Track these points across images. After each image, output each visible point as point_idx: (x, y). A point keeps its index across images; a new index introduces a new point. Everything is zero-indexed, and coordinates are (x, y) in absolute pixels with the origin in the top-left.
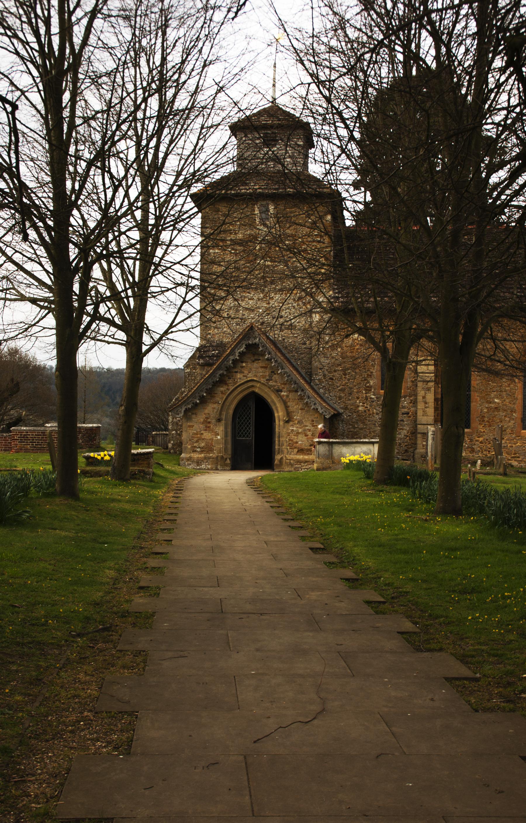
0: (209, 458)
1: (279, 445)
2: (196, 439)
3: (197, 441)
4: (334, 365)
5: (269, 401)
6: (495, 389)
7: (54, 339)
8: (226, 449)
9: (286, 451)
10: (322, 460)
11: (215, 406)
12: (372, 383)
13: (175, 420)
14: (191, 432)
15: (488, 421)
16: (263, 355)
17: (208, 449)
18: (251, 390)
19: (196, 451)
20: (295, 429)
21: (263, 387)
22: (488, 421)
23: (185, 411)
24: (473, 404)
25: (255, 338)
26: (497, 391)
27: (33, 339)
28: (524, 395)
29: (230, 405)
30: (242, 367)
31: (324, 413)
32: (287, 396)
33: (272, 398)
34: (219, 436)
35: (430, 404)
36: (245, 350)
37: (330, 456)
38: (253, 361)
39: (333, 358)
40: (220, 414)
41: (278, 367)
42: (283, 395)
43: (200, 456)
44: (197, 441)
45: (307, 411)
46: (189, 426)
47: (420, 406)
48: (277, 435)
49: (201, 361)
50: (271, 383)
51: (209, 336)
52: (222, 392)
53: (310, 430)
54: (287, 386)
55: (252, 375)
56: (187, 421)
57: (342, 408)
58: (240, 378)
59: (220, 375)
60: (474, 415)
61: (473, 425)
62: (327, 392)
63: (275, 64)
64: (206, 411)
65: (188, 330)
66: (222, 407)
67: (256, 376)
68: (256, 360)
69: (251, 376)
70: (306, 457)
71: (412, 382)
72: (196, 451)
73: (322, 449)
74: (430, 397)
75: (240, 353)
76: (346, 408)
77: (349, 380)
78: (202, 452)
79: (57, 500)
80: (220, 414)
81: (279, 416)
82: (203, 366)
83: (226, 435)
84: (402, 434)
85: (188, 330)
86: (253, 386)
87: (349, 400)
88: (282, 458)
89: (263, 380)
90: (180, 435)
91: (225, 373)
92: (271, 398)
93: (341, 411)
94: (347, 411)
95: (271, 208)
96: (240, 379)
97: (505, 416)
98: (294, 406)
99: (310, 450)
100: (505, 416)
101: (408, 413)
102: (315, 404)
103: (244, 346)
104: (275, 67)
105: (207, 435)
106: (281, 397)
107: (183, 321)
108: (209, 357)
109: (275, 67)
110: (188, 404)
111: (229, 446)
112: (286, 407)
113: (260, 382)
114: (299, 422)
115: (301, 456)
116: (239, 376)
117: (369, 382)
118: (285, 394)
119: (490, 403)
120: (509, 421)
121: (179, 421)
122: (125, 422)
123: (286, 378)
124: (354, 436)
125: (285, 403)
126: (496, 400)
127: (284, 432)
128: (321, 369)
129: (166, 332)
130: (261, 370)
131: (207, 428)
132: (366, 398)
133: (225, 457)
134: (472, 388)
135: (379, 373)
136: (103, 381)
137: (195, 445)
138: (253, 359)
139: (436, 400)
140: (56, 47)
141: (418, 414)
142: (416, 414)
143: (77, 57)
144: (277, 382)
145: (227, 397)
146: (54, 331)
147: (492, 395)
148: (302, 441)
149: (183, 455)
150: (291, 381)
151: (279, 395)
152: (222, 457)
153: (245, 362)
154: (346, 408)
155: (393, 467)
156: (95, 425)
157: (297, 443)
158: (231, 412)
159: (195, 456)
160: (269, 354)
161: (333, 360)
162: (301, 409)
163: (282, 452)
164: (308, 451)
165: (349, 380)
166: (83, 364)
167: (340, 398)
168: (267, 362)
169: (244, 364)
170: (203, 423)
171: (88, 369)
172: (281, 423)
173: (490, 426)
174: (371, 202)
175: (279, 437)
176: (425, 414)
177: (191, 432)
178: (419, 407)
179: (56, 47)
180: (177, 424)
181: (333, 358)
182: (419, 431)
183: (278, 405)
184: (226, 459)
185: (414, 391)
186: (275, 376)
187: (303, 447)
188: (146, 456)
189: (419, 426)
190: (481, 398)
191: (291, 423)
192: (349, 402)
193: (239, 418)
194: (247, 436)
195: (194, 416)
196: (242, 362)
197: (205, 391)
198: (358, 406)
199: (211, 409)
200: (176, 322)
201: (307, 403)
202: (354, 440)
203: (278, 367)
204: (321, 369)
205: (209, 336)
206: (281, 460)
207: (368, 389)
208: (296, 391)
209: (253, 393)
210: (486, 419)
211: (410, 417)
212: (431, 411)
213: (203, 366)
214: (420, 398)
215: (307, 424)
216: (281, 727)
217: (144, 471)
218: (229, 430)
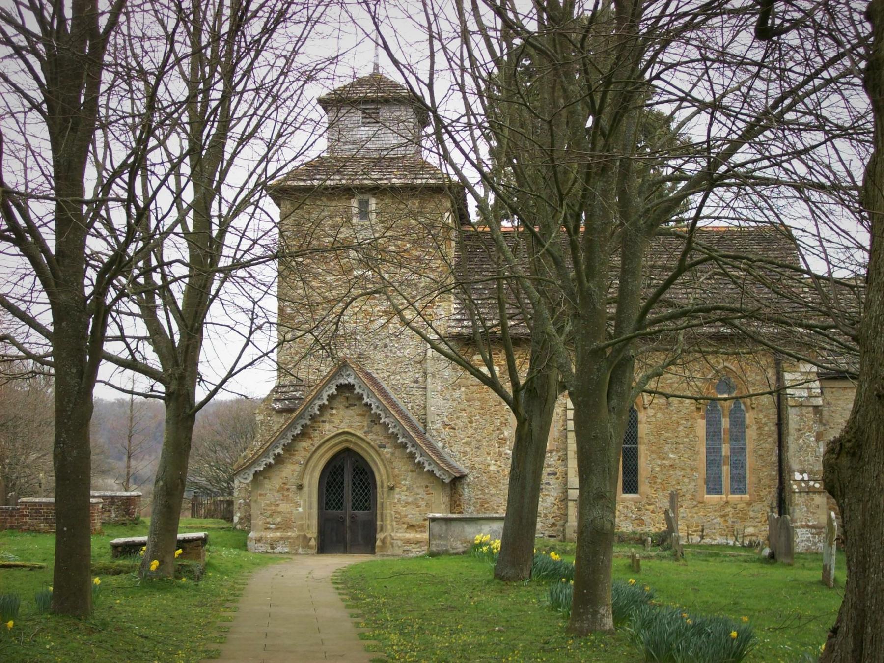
0: (288, 538)
2: (269, 512)
3: (271, 516)
12: (506, 433)
19: (269, 529)
30: (332, 415)
36: (335, 393)
44: (271, 516)
52: (305, 449)
58: (328, 429)
67: (350, 427)
70: (418, 536)
76: (473, 468)
77: (476, 429)
84: (548, 501)
86: (346, 441)
96: (329, 431)
101: (555, 474)
105: (284, 507)
116: (327, 426)
119: (664, 459)
120: (689, 483)
126: (671, 456)
131: (286, 498)
132: (500, 455)
134: (639, 440)
137: (268, 520)
141: (569, 475)
142: (566, 474)
154: (473, 468)
159: (270, 535)
165: (476, 429)
169: (334, 411)
170: (278, 491)
173: (664, 490)
184: (310, 539)
187: (414, 523)
195: (266, 481)
196: (332, 408)
199: (289, 471)
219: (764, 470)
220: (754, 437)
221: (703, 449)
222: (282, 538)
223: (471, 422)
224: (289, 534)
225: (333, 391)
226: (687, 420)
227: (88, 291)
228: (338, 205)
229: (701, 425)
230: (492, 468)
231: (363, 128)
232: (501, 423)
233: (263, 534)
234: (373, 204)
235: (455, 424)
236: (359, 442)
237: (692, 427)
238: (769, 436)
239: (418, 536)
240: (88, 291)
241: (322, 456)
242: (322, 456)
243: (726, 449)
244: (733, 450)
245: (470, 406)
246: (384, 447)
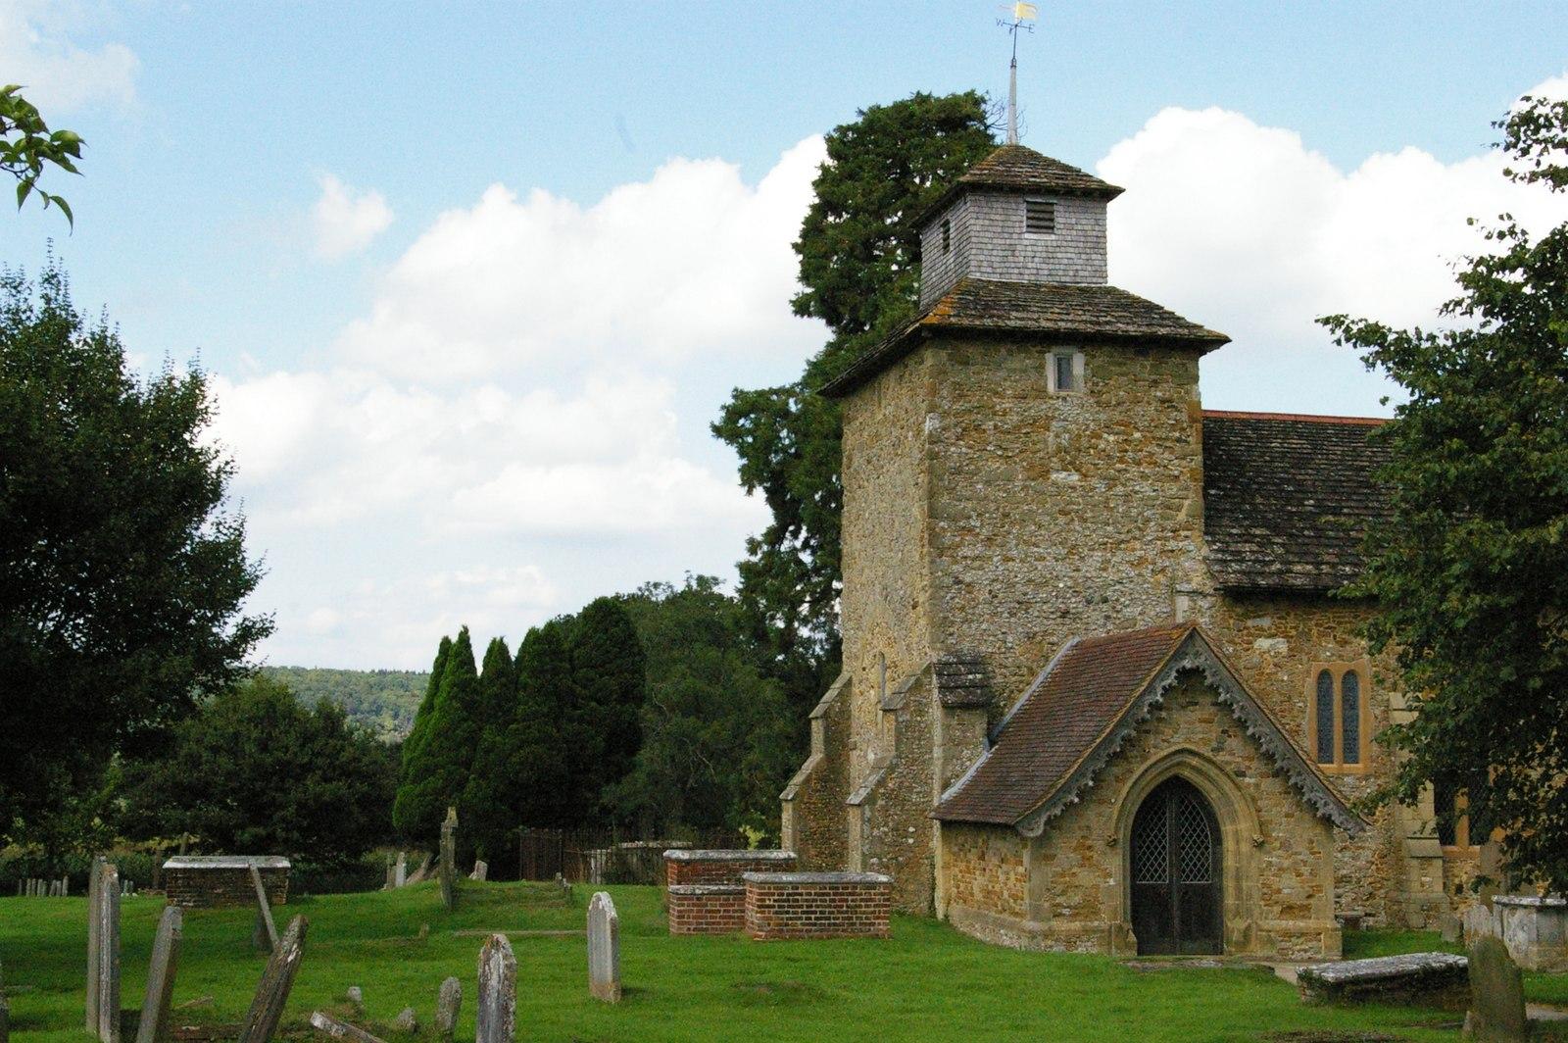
0: (1095, 931)
1: (1238, 897)
2: (1060, 888)
19: (1060, 915)
32: (1257, 786)
44: (1063, 893)
51: (951, 640)
53: (1305, 863)
55: (1189, 732)
63: (1014, 60)
70: (1301, 924)
72: (1060, 915)
78: (1074, 916)
88: (1249, 927)
99: (1307, 908)
104: (1013, 66)
105: (1086, 878)
109: (1013, 66)
115: (1291, 923)
118: (1253, 781)
130: (1199, 727)
131: (1086, 862)
148: (1290, 887)
152: (1120, 928)
157: (1279, 891)
162: (1287, 815)
163: (1249, 913)
164: (1303, 910)
170: (1075, 850)
172: (1245, 847)
175: (1238, 879)
197: (1090, 775)
205: (951, 640)
206: (1246, 934)
209: (1176, 778)
215: (1300, 849)
222: (1086, 931)
224: (1096, 923)
225: (1171, 680)
228: (1020, 361)
231: (1027, 236)
233: (1055, 924)
234: (1078, 364)
236: (1206, 767)
239: (1301, 924)
246: (1243, 774)
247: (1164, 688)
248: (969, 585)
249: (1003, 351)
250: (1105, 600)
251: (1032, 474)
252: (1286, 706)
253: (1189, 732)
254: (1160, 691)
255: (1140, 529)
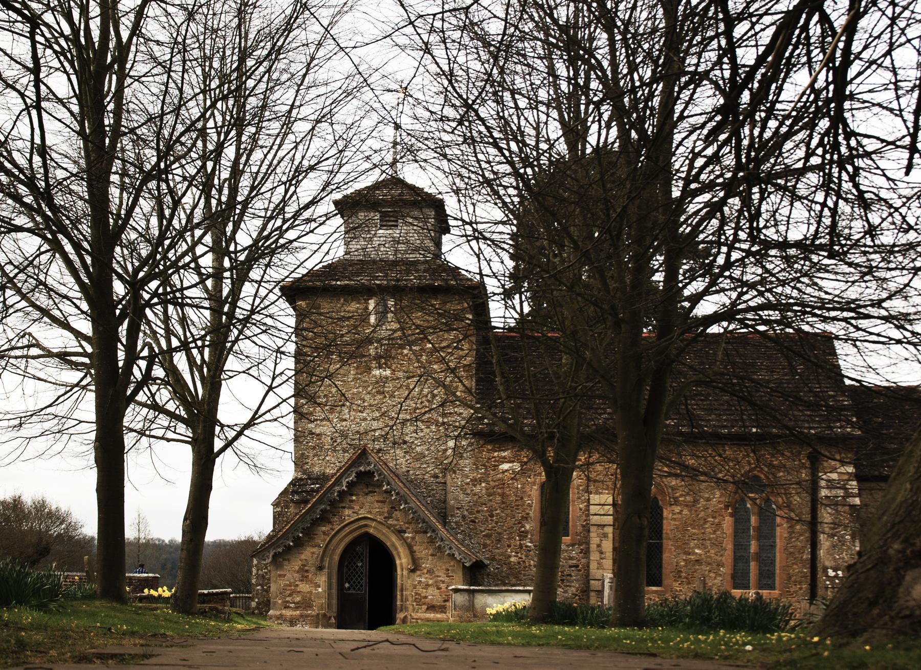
0: (307, 616)
1: (402, 601)
2: (289, 592)
4: (476, 503)
5: (388, 544)
6: (695, 537)
7: (93, 436)
8: (329, 605)
9: (411, 607)
10: (460, 612)
11: (315, 550)
12: (528, 527)
13: (260, 572)
14: (282, 582)
15: (686, 578)
16: (381, 486)
17: (306, 604)
18: (363, 530)
19: (289, 607)
20: (423, 580)
21: (380, 527)
22: (686, 578)
23: (274, 557)
24: (665, 556)
25: (369, 464)
26: (699, 540)
27: (66, 437)
28: (735, 545)
29: (334, 550)
30: (352, 501)
31: (463, 560)
32: (413, 538)
33: (392, 541)
34: (319, 588)
35: (607, 554)
36: (355, 480)
37: (471, 607)
38: (367, 494)
39: (475, 495)
40: (322, 560)
41: (400, 501)
42: (408, 537)
43: (294, 613)
44: (290, 595)
45: (440, 558)
46: (280, 576)
47: (594, 556)
48: (399, 588)
49: (296, 497)
50: (390, 522)
52: (324, 533)
54: (413, 526)
55: (364, 510)
56: (277, 569)
57: (487, 559)
58: (348, 514)
59: (322, 510)
60: (667, 569)
61: (666, 582)
62: (467, 538)
64: (303, 557)
65: (275, 420)
66: (324, 552)
67: (370, 512)
68: (370, 492)
69: (363, 513)
70: (439, 616)
71: (583, 526)
72: (289, 607)
73: (460, 599)
74: (608, 546)
75: (348, 482)
76: (493, 559)
77: (496, 523)
78: (296, 608)
79: (97, 603)
80: (322, 560)
81: (401, 564)
82: (298, 503)
83: (330, 587)
84: (570, 592)
85: (275, 420)
86: (366, 526)
87: (497, 548)
88: (406, 617)
89: (379, 518)
90: (268, 591)
91: (328, 508)
92: (390, 540)
93: (487, 562)
94: (494, 563)
95: (391, 303)
96: (349, 516)
97: (710, 571)
98: (422, 551)
100: (710, 571)
101: (577, 566)
102: (451, 548)
103: (354, 474)
105: (304, 587)
106: (405, 540)
107: (269, 411)
108: (306, 492)
110: (278, 547)
111: (334, 602)
112: (412, 552)
113: (376, 520)
114: (428, 571)
116: (347, 512)
117: (524, 526)
118: (410, 535)
119: (689, 554)
120: (715, 578)
121: (266, 573)
122: (191, 540)
123: (411, 516)
124: (505, 581)
125: (410, 547)
126: (697, 551)
127: (408, 583)
128: (458, 509)
129: (248, 426)
130: (377, 505)
131: (304, 578)
132: (521, 546)
133: (328, 615)
134: (664, 536)
135: (538, 515)
136: (164, 556)
137: (287, 599)
138: (367, 491)
139: (614, 549)
140: (96, 34)
141: (591, 567)
142: (588, 567)
143: (123, 50)
144: (399, 519)
145: (332, 539)
146: (94, 426)
147: (692, 544)
148: (433, 595)
149: (271, 612)
150: (418, 519)
151: (403, 537)
152: (325, 615)
153: (356, 495)
154: (493, 559)
155: (555, 601)
156: (151, 575)
157: (426, 597)
158: (336, 558)
159: (288, 613)
160: (388, 484)
161: (475, 498)
162: (432, 555)
163: (407, 609)
165: (496, 523)
166: (136, 535)
167: (485, 546)
168: (385, 495)
169: (354, 498)
170: (298, 572)
171: (143, 541)
172: (405, 573)
173: (689, 583)
174: (528, 315)
175: (402, 590)
176: (600, 566)
177: (282, 582)
178: (592, 558)
179: (96, 34)
180: (263, 577)
181: (475, 495)
182: (592, 588)
183: (401, 550)
184: (330, 617)
185: (586, 538)
186: (396, 513)
187: (435, 603)
188: (220, 597)
189: (592, 582)
190: (677, 548)
191: (418, 573)
192: (497, 551)
193: (347, 566)
194: (359, 589)
195: (286, 563)
196: (352, 495)
198: (510, 556)
199: (309, 554)
200: (260, 413)
201: (439, 547)
202: (504, 588)
203: (400, 501)
204: (458, 509)
207: (523, 535)
208: (425, 532)
209: (367, 534)
210: (683, 575)
211: (580, 571)
212: (608, 563)
213: (298, 503)
214: (593, 547)
216: (387, 641)
217: (216, 609)
218: (334, 581)
219: (795, 566)
220: (785, 535)
221: (729, 546)
223: (492, 516)
226: (714, 518)
227: (121, 364)
229: (728, 523)
230: (512, 559)
232: (522, 517)
235: (476, 518)
237: (719, 524)
238: (801, 535)
240: (121, 364)
241: (342, 540)
242: (342, 540)
243: (753, 547)
244: (761, 547)
245: (491, 500)
247: (348, 482)
248: (318, 435)
249: (342, 300)
250: (405, 442)
251: (359, 371)
252: (519, 503)
253: (364, 510)
254: (344, 484)
255: (428, 401)
